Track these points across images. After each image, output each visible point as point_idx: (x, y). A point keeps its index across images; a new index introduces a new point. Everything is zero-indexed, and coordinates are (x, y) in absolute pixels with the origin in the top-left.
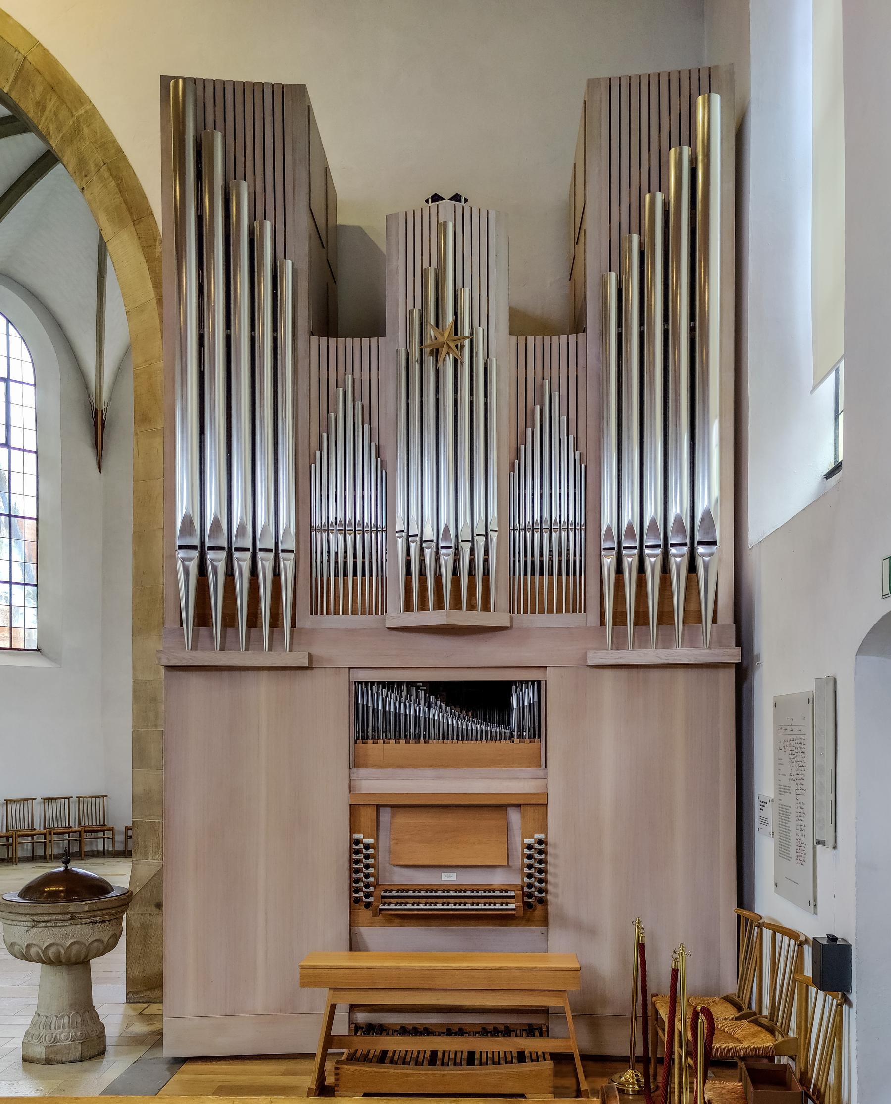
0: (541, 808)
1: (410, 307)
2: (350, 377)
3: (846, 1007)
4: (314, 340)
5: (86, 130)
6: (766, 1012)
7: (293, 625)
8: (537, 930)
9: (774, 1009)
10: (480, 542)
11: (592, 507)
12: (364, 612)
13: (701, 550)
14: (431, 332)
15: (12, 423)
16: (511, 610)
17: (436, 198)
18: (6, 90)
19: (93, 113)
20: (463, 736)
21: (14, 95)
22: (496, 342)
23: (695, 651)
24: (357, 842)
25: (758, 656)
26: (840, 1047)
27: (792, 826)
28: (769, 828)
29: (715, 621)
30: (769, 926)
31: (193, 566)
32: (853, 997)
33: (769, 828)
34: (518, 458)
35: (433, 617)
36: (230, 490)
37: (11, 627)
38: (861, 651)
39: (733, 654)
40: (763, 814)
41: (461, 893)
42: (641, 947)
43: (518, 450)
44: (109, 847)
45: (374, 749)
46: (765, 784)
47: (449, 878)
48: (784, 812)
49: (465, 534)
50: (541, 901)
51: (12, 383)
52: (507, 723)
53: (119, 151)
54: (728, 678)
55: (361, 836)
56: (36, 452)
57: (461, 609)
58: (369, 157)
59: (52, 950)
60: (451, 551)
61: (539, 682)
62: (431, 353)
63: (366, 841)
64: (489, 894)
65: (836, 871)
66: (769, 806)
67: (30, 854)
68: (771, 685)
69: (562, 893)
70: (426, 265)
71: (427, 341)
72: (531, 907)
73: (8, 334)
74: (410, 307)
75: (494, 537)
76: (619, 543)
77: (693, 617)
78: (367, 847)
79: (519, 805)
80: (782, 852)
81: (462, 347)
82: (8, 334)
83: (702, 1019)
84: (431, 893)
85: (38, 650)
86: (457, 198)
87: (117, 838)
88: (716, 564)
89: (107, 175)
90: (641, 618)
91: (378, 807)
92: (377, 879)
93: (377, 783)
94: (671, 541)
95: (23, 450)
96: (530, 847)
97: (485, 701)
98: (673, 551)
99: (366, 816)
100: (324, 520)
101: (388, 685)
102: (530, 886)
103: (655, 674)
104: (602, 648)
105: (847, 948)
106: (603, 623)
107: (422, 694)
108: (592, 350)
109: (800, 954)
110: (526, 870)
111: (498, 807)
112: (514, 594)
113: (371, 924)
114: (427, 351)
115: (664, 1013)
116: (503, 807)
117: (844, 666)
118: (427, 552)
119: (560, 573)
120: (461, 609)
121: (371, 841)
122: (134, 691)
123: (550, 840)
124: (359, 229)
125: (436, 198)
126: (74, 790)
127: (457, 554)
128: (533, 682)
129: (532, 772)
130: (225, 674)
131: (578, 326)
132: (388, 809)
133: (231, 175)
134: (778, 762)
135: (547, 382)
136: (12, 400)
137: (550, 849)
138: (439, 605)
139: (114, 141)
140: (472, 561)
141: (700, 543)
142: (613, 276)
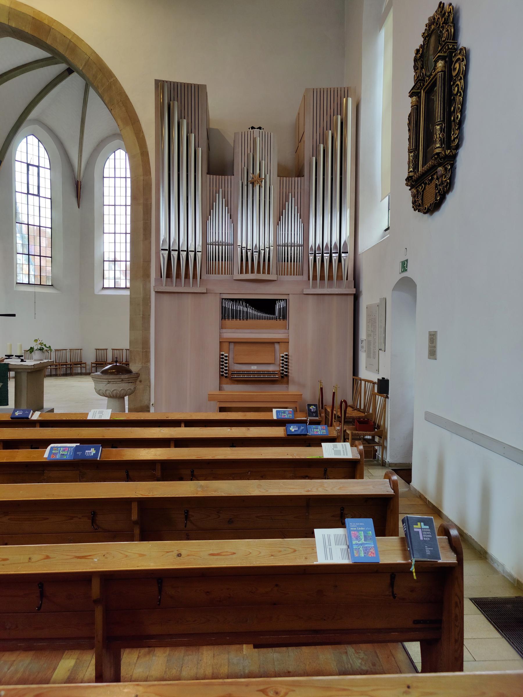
0: (287, 343)
1: (243, 166)
2: (221, 190)
3: (387, 399)
4: (208, 176)
5: (113, 87)
6: (362, 407)
7: (200, 278)
8: (285, 386)
9: (365, 406)
10: (267, 250)
11: (306, 237)
12: (225, 274)
13: (343, 255)
14: (251, 175)
15: (41, 186)
16: (277, 274)
17: (253, 128)
18: (81, 69)
19: (116, 81)
20: (265, 318)
21: (84, 71)
22: (272, 179)
23: (340, 290)
24: (223, 355)
25: (361, 291)
26: (385, 411)
27: (372, 347)
28: (364, 349)
29: (347, 279)
30: (364, 380)
31: (166, 256)
32: (389, 396)
33: (364, 349)
34: (280, 220)
35: (250, 276)
36: (180, 229)
37: (40, 275)
38: (393, 290)
39: (353, 291)
40: (362, 345)
41: (258, 373)
42: (322, 389)
43: (280, 218)
44: (84, 371)
45: (229, 322)
46: (363, 335)
47: (254, 368)
48: (369, 343)
49: (262, 247)
50: (286, 375)
51: (40, 168)
52: (274, 313)
53: (127, 96)
54: (352, 298)
55: (223, 353)
56: (51, 199)
57: (260, 273)
58: (224, 108)
59: (115, 392)
60: (257, 253)
61: (286, 300)
62: (251, 183)
63: (225, 355)
64: (269, 373)
65: (384, 358)
66: (364, 342)
67: (49, 374)
68: (365, 302)
69: (293, 372)
70: (249, 152)
71: (250, 179)
72: (283, 378)
73: (39, 146)
74: (243, 166)
75: (272, 248)
76: (315, 251)
77: (340, 277)
78: (226, 356)
79: (279, 342)
80: (368, 356)
81: (262, 181)
82: (39, 146)
83: (343, 403)
84: (248, 373)
85: (52, 285)
86: (260, 128)
87: (87, 367)
88: (347, 258)
89: (122, 105)
90: (322, 278)
91: (230, 342)
92: (229, 368)
93: (230, 334)
94: (333, 252)
95: (45, 198)
96: (283, 357)
97: (266, 307)
98: (334, 255)
99: (226, 345)
100: (214, 240)
101: (232, 300)
102: (283, 370)
103: (326, 297)
104: (309, 288)
105: (388, 381)
106: (309, 279)
107: (244, 303)
108: (306, 183)
109: (374, 387)
110: (281, 365)
111: (272, 343)
112: (285, 268)
113: (227, 384)
114: (249, 183)
115: (329, 410)
116: (273, 343)
117: (388, 295)
118: (249, 253)
119: (291, 261)
120: (260, 273)
121: (227, 355)
122: (130, 302)
123: (290, 354)
124: (217, 130)
125: (253, 128)
126: (68, 346)
127: (259, 254)
128: (284, 300)
129: (283, 331)
130: (176, 295)
131: (300, 174)
132: (233, 344)
133: (180, 118)
134: (368, 326)
135: (290, 194)
136: (41, 175)
137: (290, 358)
138: (252, 272)
139: (125, 92)
140: (264, 256)
141: (343, 253)
142: (314, 158)
